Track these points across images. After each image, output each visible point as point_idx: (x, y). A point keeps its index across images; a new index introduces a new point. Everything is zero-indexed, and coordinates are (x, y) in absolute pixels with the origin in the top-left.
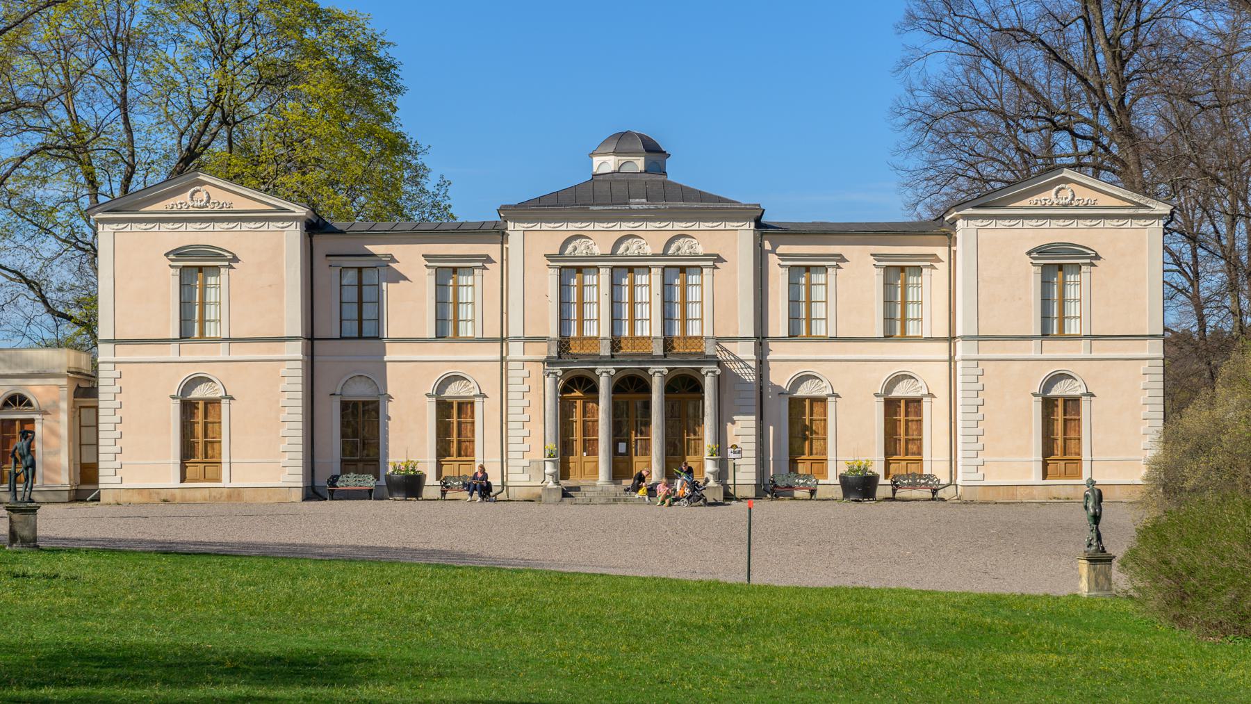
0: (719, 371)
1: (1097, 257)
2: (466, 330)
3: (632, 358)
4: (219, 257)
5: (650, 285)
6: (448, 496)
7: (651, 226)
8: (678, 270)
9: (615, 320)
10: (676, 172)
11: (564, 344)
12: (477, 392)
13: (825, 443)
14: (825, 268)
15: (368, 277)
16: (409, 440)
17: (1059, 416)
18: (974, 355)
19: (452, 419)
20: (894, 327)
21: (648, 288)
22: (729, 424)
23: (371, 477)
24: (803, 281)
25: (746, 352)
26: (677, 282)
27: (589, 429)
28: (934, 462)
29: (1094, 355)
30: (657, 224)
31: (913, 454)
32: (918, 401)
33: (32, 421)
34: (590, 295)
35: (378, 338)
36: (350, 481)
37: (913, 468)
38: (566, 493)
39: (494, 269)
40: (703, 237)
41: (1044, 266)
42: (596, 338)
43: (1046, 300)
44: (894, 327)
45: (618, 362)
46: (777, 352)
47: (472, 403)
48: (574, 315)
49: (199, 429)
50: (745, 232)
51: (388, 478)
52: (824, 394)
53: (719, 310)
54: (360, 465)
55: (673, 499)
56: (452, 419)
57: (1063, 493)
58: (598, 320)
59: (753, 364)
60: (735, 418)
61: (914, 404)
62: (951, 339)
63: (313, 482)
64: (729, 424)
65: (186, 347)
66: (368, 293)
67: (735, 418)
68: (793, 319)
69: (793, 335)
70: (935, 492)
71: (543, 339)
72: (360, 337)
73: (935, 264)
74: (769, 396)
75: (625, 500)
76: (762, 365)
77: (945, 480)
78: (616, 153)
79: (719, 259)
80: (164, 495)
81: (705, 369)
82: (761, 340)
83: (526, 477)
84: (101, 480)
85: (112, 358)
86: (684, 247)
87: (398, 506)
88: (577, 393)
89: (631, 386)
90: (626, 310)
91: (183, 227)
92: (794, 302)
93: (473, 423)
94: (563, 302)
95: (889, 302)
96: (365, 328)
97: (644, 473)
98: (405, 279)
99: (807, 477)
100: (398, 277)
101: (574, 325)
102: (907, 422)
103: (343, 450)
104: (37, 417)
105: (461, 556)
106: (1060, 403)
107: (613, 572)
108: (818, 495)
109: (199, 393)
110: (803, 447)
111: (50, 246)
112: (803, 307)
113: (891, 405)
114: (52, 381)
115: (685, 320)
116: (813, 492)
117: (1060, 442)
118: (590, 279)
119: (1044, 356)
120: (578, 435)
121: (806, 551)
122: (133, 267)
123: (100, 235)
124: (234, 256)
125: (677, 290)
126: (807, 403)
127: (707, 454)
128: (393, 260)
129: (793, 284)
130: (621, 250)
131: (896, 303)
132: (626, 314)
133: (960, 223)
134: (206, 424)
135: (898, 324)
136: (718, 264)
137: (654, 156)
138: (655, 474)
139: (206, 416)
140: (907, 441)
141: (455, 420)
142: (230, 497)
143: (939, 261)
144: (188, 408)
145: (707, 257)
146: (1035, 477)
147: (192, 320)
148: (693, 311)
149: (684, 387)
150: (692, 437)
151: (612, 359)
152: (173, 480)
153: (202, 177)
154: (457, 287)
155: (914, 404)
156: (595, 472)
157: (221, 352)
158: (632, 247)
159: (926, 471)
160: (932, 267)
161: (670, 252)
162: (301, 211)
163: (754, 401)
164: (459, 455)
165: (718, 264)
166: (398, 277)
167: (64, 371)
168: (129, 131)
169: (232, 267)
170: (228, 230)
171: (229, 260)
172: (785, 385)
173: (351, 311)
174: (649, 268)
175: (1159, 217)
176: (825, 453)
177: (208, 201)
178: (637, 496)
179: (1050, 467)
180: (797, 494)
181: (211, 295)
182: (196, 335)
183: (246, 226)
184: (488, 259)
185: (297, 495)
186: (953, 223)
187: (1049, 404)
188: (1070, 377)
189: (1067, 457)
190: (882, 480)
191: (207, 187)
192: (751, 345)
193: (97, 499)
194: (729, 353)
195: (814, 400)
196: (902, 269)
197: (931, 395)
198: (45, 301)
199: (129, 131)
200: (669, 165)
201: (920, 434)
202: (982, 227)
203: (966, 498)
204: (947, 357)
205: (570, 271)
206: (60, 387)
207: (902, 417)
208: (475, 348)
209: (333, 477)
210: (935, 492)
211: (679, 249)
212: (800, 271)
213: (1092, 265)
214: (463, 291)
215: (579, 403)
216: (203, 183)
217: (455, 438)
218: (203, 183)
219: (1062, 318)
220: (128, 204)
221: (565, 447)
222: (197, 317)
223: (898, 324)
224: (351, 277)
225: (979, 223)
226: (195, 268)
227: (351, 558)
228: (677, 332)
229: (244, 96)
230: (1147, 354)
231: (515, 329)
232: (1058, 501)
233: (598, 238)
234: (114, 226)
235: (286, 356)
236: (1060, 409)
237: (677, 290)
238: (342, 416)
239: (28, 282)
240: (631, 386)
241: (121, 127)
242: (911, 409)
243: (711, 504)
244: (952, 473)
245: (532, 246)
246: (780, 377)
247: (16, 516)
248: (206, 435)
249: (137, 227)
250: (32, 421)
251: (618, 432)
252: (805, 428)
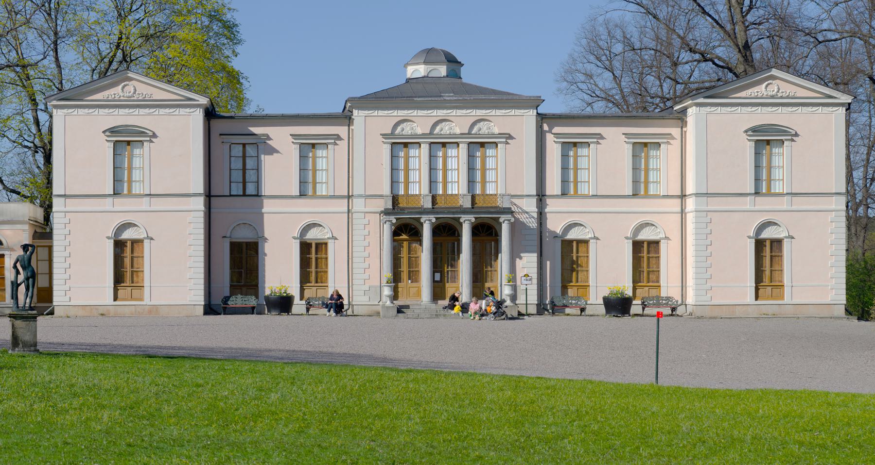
0: (513, 220)
1: (796, 135)
2: (322, 190)
3: (450, 210)
4: (142, 134)
5: (458, 157)
6: (310, 312)
8: (479, 146)
11: (395, 199)
12: (329, 235)
13: (588, 274)
14: (588, 144)
15: (250, 151)
16: (280, 272)
17: (767, 252)
18: (705, 208)
19: (311, 255)
21: (457, 159)
22: (518, 260)
23: (254, 297)
24: (440, 154)
25: (530, 206)
26: (478, 154)
27: (413, 263)
28: (669, 287)
30: (464, 111)
31: (653, 282)
32: (657, 243)
35: (257, 195)
36: (237, 301)
37: (653, 293)
38: (400, 310)
39: (343, 144)
40: (497, 121)
41: (757, 141)
42: (496, 195)
43: (757, 167)
45: (437, 213)
46: (551, 206)
47: (326, 244)
49: (127, 261)
51: (267, 298)
52: (142, 237)
53: (509, 178)
54: (244, 289)
55: (483, 314)
56: (311, 255)
57: (771, 310)
58: (420, 182)
59: (535, 215)
60: (522, 255)
61: (654, 245)
62: (683, 196)
63: (210, 302)
64: (518, 260)
65: (118, 200)
67: (522, 255)
68: (565, 181)
69: (564, 194)
70: (673, 309)
72: (244, 195)
73: (600, 141)
74: (547, 239)
75: (445, 315)
76: (541, 215)
79: (510, 137)
81: (503, 218)
82: (541, 197)
83: (366, 298)
84: (55, 299)
85: (63, 209)
86: (484, 128)
87: (273, 320)
88: (404, 237)
89: (446, 232)
90: (402, 174)
91: (116, 111)
92: (565, 168)
93: (327, 258)
94: (394, 169)
95: (635, 169)
96: (249, 191)
97: (456, 295)
98: (277, 152)
99: (578, 298)
100: (272, 151)
102: (648, 258)
103: (232, 280)
105: (357, 357)
106: (768, 244)
108: (587, 312)
109: (127, 235)
110: (571, 277)
112: (571, 173)
113: (637, 246)
114: (19, 226)
115: (484, 182)
116: (583, 310)
119: (757, 208)
120: (404, 268)
121: (576, 352)
123: (54, 117)
124: (154, 133)
125: (440, 161)
126: (575, 244)
127: (504, 282)
128: (269, 138)
129: (565, 156)
130: (437, 130)
131: (640, 170)
132: (478, 178)
134: (132, 258)
135: (642, 186)
136: (337, 142)
138: (465, 295)
139: (132, 252)
140: (648, 273)
141: (313, 256)
142: (150, 312)
143: (673, 138)
144: (119, 245)
147: (121, 181)
149: (486, 232)
150: (489, 269)
151: (432, 211)
152: (109, 298)
153: (131, 75)
155: (654, 245)
156: (419, 294)
158: (445, 129)
159: (663, 294)
160: (668, 143)
161: (397, 132)
162: (204, 101)
163: (536, 243)
164: (317, 282)
165: (337, 142)
166: (272, 151)
167: (27, 219)
169: (152, 142)
170: (149, 114)
171: (150, 136)
172: (559, 230)
173: (237, 176)
174: (458, 144)
175: (842, 105)
176: (587, 281)
177: (135, 93)
178: (452, 312)
179: (761, 292)
181: (137, 162)
182: (125, 192)
183: (163, 111)
184: (338, 137)
186: (684, 111)
187: (759, 244)
188: (775, 224)
189: (773, 284)
190: (297, 300)
191: (133, 82)
192: (534, 201)
193: (52, 313)
194: (518, 207)
195: (579, 242)
197: (667, 238)
201: (658, 266)
202: (710, 113)
203: (699, 314)
204: (679, 209)
205: (400, 145)
206: (24, 230)
208: (331, 204)
209: (225, 297)
210: (673, 309)
211: (480, 129)
212: (569, 146)
213: (793, 140)
215: (405, 244)
216: (131, 79)
217: (313, 269)
218: (131, 79)
220: (71, 96)
221: (396, 278)
222: (126, 179)
223: (642, 186)
224: (237, 151)
226: (124, 141)
227: (292, 359)
230: (833, 207)
232: (766, 317)
233: (419, 122)
234: (65, 111)
235: (191, 208)
236: (768, 248)
237: (440, 161)
238: (231, 253)
240: (446, 232)
242: (652, 249)
243: (510, 319)
244: (683, 295)
245: (372, 125)
246: (555, 225)
248: (132, 267)
251: (437, 266)
252: (573, 262)
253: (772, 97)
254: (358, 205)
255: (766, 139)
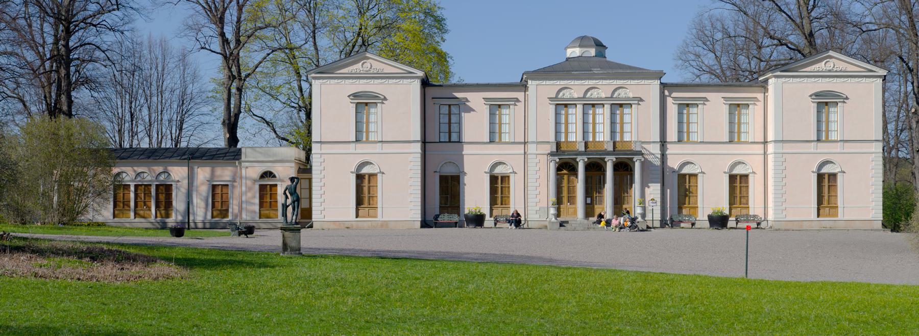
1: (847, 98)
2: (506, 138)
7: (605, 82)
8: (618, 106)
9: (585, 132)
10: (611, 55)
11: (558, 145)
12: (511, 171)
14: (697, 105)
16: (476, 197)
17: (826, 183)
19: (498, 185)
20: (734, 137)
21: (602, 116)
25: (656, 149)
28: (755, 207)
29: (845, 151)
32: (747, 176)
33: (276, 185)
34: (572, 119)
36: (445, 218)
37: (744, 212)
39: (521, 105)
40: (631, 88)
44: (734, 137)
46: (671, 149)
48: (563, 130)
49: (366, 189)
50: (653, 87)
51: (466, 216)
53: (640, 129)
56: (498, 185)
57: (828, 225)
59: (659, 156)
61: (745, 177)
62: (765, 142)
65: (359, 145)
66: (454, 119)
68: (680, 132)
69: (680, 141)
71: (548, 142)
72: (450, 141)
74: (667, 173)
76: (663, 156)
77: (762, 216)
78: (580, 46)
79: (641, 100)
80: (347, 225)
81: (635, 158)
82: (663, 143)
83: (538, 216)
84: (313, 216)
85: (319, 152)
86: (622, 93)
87: (470, 231)
88: (565, 172)
89: (595, 168)
91: (358, 81)
92: (680, 123)
94: (557, 123)
95: (731, 123)
96: (454, 139)
99: (690, 216)
100: (470, 110)
101: (563, 136)
103: (441, 203)
104: (278, 183)
105: (531, 258)
106: (826, 177)
107: (642, 270)
108: (697, 226)
109: (365, 170)
111: (278, 105)
112: (685, 126)
113: (732, 178)
114: (288, 164)
115: (622, 132)
116: (693, 224)
117: (826, 198)
118: (571, 111)
120: (565, 194)
122: (331, 99)
128: (468, 101)
129: (680, 114)
130: (588, 95)
133: (770, 81)
137: (600, 49)
138: (608, 215)
139: (369, 182)
140: (740, 198)
141: (499, 185)
142: (382, 226)
143: (758, 101)
145: (634, 98)
146: (813, 215)
147: (361, 131)
148: (627, 128)
149: (624, 168)
153: (368, 55)
154: (500, 115)
156: (575, 213)
157: (378, 148)
158: (594, 94)
159: (751, 213)
160: (755, 104)
162: (421, 74)
163: (660, 176)
166: (470, 110)
168: (316, 49)
172: (676, 167)
173: (445, 128)
179: (821, 211)
180: (682, 225)
183: (391, 81)
184: (517, 100)
185: (419, 224)
186: (766, 81)
187: (820, 177)
188: (832, 162)
192: (658, 146)
193: (311, 227)
195: (691, 175)
196: (738, 105)
198: (275, 132)
199: (316, 49)
200: (608, 53)
202: (785, 82)
205: (562, 106)
207: (738, 184)
208: (513, 148)
210: (759, 224)
212: (684, 106)
214: (504, 117)
215: (566, 177)
216: (368, 58)
217: (499, 195)
219: (827, 131)
220: (326, 70)
221: (559, 202)
224: (445, 110)
225: (783, 80)
226: (364, 103)
228: (618, 139)
229: (372, 33)
230: (873, 150)
231: (531, 137)
232: (825, 229)
233: (576, 89)
235: (412, 151)
239: (267, 123)
240: (595, 168)
241: (313, 48)
243: (643, 230)
244: (766, 214)
245: (541, 92)
246: (673, 163)
247: (287, 234)
249: (332, 81)
250: (276, 185)
251: (588, 192)
252: (686, 190)
253: (830, 71)
254: (532, 148)
255: (825, 102)
